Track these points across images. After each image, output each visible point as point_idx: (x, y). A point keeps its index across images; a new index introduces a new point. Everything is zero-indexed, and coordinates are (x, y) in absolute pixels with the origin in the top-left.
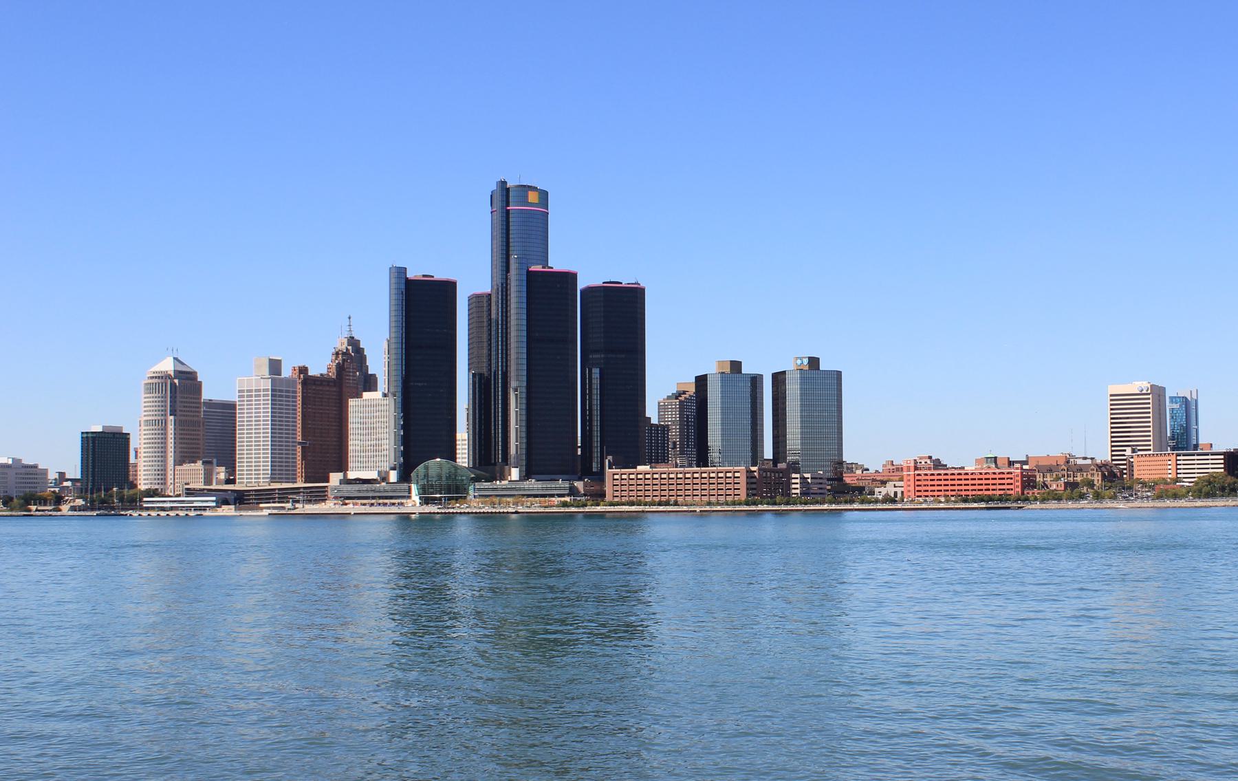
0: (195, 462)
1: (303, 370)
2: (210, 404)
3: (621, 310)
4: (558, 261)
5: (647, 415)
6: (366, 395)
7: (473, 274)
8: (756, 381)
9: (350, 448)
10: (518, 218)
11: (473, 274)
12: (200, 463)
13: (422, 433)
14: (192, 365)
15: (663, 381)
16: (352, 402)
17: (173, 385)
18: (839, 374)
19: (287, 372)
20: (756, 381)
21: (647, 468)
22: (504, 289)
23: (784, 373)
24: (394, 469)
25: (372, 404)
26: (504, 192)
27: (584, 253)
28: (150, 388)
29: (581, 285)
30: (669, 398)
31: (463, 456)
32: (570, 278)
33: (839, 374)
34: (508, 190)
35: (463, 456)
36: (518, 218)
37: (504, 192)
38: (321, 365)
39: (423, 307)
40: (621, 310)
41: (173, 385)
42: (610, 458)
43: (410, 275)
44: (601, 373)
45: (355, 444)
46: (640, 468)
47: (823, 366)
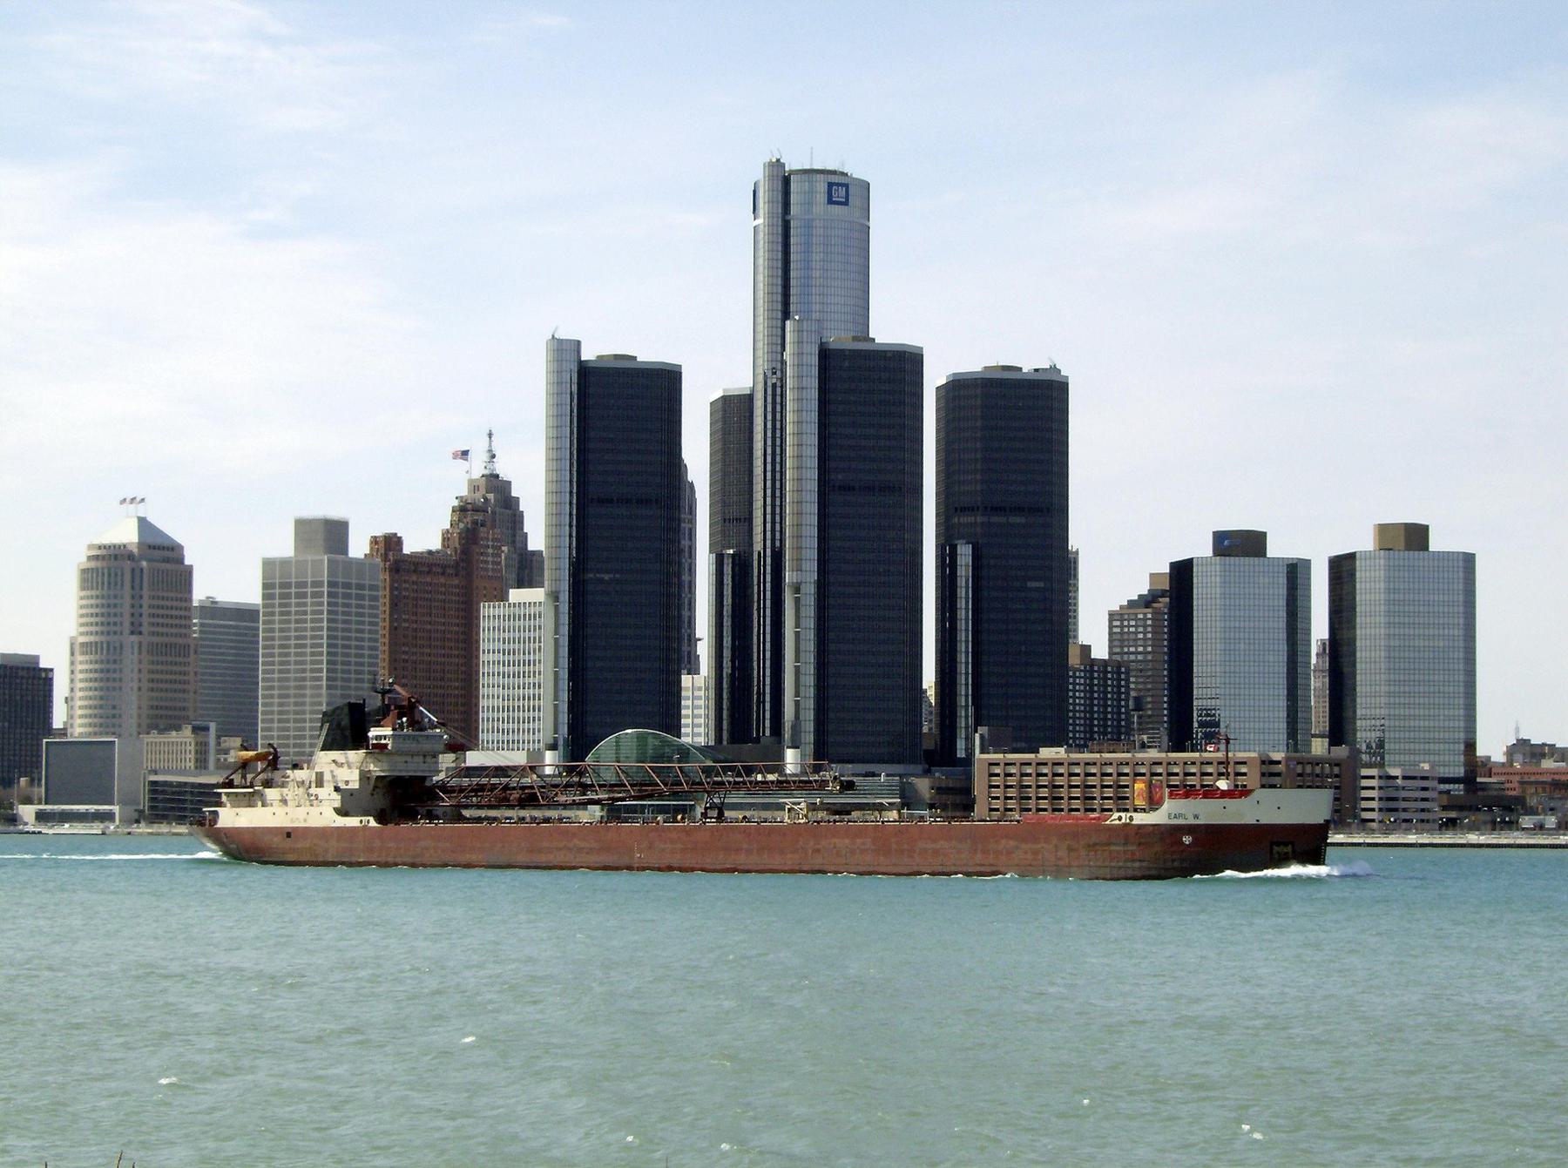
0: (178, 728)
1: (390, 544)
2: (213, 610)
3: (1018, 423)
4: (887, 327)
5: (514, 494)
6: (515, 595)
7: (714, 347)
8: (1296, 572)
9: (483, 703)
10: (811, 226)
11: (714, 347)
12: (187, 731)
13: (616, 666)
14: (174, 529)
15: (1111, 565)
16: (488, 611)
17: (137, 573)
18: (1469, 560)
19: (358, 547)
20: (1296, 572)
21: (1058, 753)
22: (778, 369)
23: (1191, 560)
24: (553, 747)
25: (526, 614)
26: (783, 181)
27: (941, 313)
28: (89, 578)
29: (934, 378)
30: (1131, 604)
31: (697, 722)
32: (906, 363)
33: (1469, 560)
34: (786, 181)
35: (697, 722)
36: (811, 226)
37: (783, 181)
38: (425, 535)
39: (615, 411)
40: (1018, 423)
41: (137, 573)
42: (983, 730)
43: (588, 354)
44: (976, 557)
45: (491, 694)
46: (1046, 753)
47: (1436, 544)
